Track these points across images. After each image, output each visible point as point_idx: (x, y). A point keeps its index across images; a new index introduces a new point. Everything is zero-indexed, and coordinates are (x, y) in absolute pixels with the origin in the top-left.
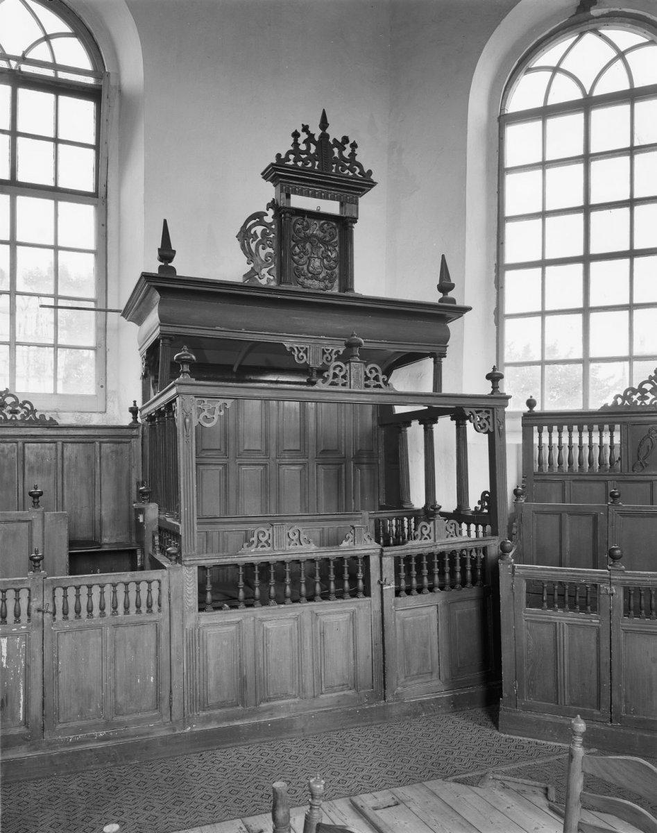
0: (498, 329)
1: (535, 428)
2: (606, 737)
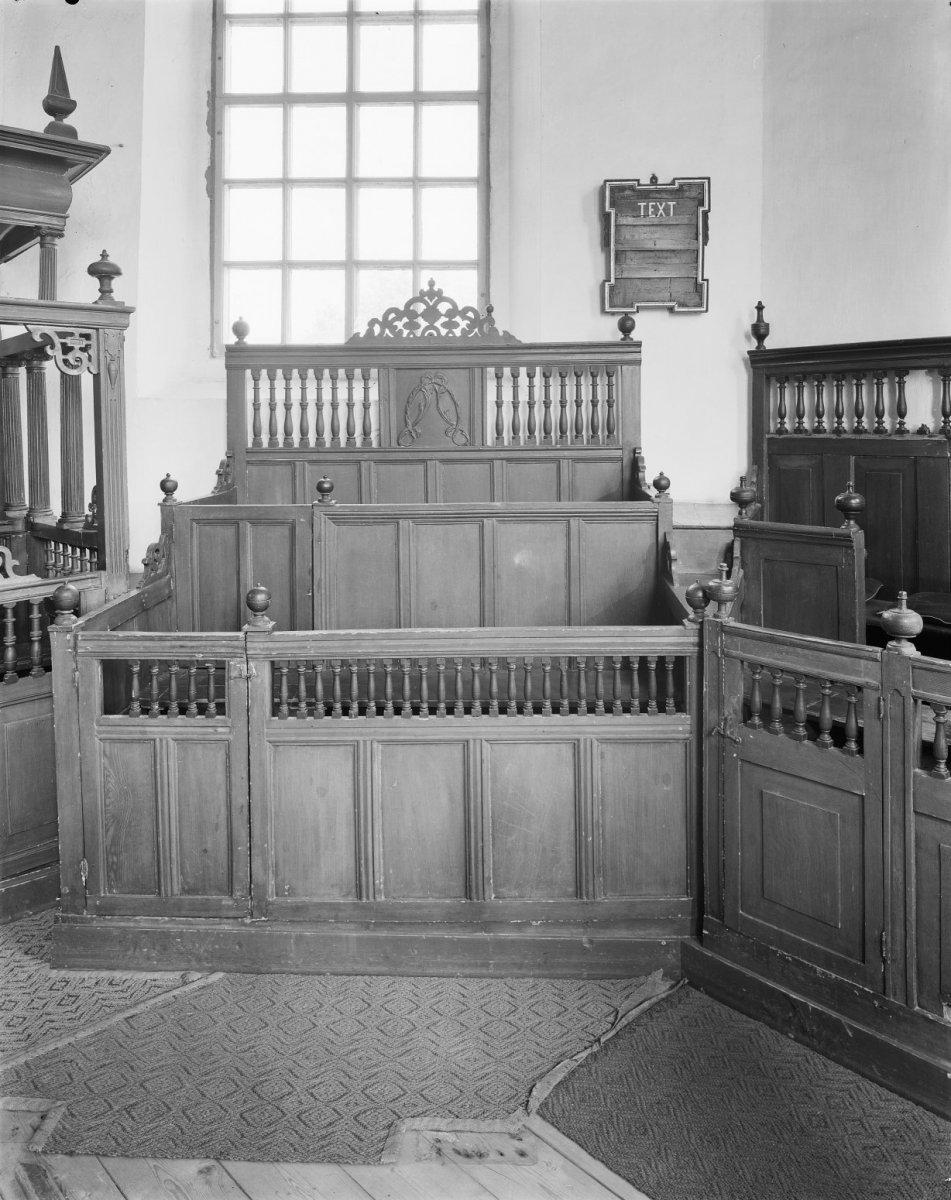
0: (212, 203)
1: (248, 372)
2: (240, 947)
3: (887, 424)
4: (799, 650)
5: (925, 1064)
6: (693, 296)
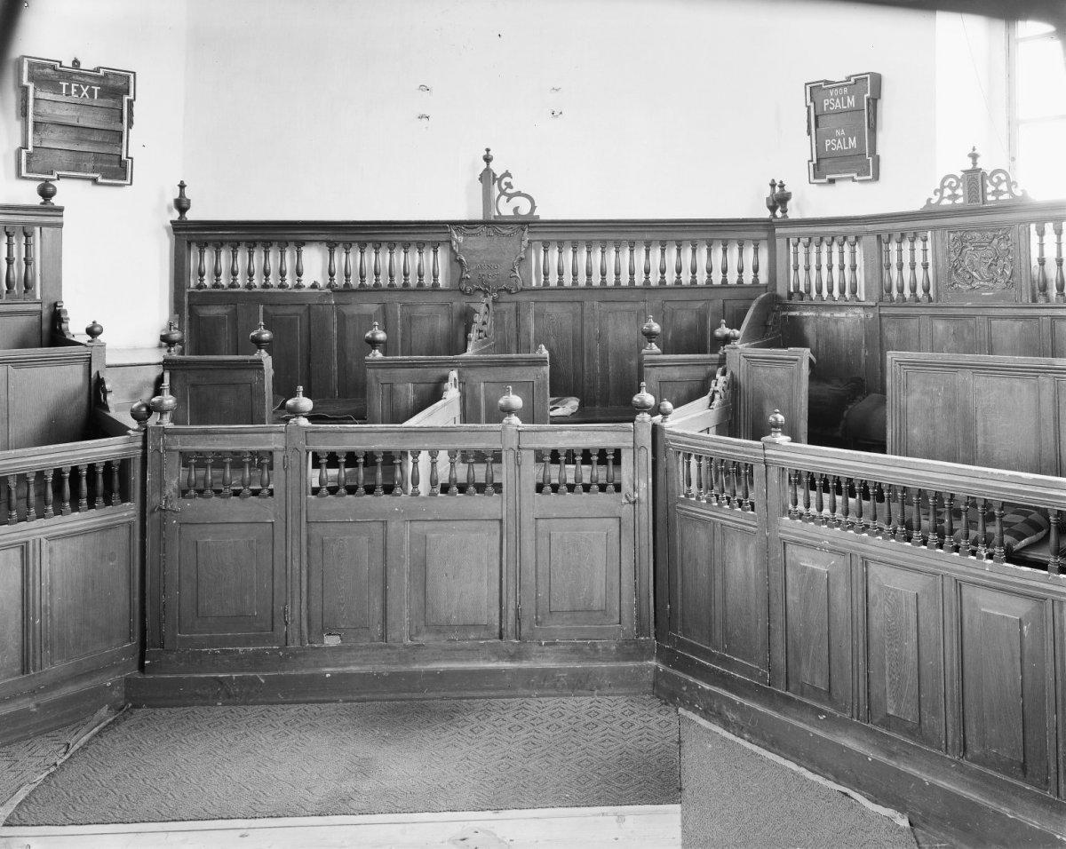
3: (289, 281)
4: (227, 436)
5: (313, 675)
6: (116, 169)
